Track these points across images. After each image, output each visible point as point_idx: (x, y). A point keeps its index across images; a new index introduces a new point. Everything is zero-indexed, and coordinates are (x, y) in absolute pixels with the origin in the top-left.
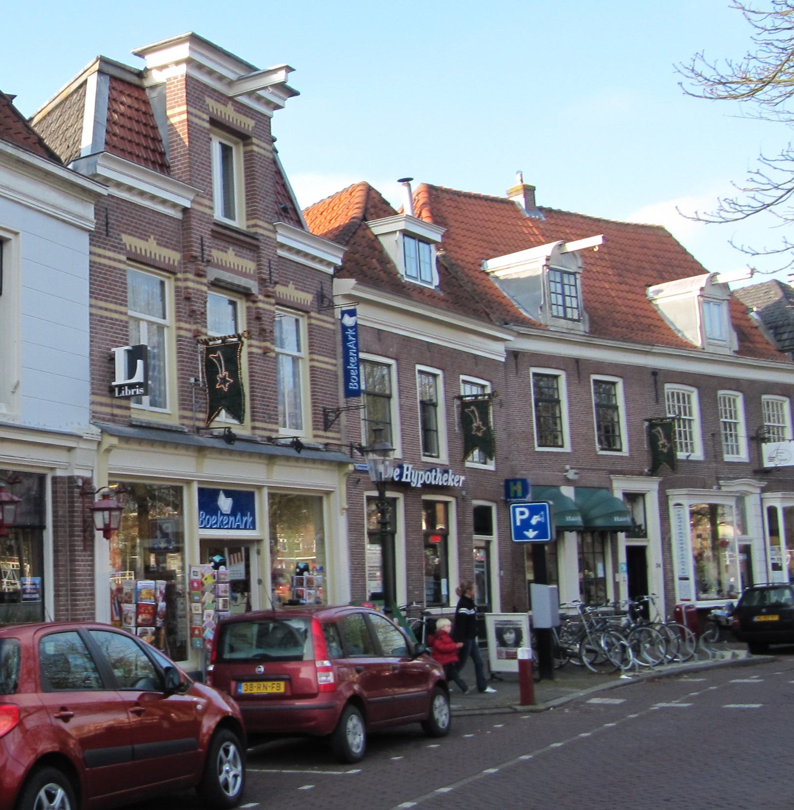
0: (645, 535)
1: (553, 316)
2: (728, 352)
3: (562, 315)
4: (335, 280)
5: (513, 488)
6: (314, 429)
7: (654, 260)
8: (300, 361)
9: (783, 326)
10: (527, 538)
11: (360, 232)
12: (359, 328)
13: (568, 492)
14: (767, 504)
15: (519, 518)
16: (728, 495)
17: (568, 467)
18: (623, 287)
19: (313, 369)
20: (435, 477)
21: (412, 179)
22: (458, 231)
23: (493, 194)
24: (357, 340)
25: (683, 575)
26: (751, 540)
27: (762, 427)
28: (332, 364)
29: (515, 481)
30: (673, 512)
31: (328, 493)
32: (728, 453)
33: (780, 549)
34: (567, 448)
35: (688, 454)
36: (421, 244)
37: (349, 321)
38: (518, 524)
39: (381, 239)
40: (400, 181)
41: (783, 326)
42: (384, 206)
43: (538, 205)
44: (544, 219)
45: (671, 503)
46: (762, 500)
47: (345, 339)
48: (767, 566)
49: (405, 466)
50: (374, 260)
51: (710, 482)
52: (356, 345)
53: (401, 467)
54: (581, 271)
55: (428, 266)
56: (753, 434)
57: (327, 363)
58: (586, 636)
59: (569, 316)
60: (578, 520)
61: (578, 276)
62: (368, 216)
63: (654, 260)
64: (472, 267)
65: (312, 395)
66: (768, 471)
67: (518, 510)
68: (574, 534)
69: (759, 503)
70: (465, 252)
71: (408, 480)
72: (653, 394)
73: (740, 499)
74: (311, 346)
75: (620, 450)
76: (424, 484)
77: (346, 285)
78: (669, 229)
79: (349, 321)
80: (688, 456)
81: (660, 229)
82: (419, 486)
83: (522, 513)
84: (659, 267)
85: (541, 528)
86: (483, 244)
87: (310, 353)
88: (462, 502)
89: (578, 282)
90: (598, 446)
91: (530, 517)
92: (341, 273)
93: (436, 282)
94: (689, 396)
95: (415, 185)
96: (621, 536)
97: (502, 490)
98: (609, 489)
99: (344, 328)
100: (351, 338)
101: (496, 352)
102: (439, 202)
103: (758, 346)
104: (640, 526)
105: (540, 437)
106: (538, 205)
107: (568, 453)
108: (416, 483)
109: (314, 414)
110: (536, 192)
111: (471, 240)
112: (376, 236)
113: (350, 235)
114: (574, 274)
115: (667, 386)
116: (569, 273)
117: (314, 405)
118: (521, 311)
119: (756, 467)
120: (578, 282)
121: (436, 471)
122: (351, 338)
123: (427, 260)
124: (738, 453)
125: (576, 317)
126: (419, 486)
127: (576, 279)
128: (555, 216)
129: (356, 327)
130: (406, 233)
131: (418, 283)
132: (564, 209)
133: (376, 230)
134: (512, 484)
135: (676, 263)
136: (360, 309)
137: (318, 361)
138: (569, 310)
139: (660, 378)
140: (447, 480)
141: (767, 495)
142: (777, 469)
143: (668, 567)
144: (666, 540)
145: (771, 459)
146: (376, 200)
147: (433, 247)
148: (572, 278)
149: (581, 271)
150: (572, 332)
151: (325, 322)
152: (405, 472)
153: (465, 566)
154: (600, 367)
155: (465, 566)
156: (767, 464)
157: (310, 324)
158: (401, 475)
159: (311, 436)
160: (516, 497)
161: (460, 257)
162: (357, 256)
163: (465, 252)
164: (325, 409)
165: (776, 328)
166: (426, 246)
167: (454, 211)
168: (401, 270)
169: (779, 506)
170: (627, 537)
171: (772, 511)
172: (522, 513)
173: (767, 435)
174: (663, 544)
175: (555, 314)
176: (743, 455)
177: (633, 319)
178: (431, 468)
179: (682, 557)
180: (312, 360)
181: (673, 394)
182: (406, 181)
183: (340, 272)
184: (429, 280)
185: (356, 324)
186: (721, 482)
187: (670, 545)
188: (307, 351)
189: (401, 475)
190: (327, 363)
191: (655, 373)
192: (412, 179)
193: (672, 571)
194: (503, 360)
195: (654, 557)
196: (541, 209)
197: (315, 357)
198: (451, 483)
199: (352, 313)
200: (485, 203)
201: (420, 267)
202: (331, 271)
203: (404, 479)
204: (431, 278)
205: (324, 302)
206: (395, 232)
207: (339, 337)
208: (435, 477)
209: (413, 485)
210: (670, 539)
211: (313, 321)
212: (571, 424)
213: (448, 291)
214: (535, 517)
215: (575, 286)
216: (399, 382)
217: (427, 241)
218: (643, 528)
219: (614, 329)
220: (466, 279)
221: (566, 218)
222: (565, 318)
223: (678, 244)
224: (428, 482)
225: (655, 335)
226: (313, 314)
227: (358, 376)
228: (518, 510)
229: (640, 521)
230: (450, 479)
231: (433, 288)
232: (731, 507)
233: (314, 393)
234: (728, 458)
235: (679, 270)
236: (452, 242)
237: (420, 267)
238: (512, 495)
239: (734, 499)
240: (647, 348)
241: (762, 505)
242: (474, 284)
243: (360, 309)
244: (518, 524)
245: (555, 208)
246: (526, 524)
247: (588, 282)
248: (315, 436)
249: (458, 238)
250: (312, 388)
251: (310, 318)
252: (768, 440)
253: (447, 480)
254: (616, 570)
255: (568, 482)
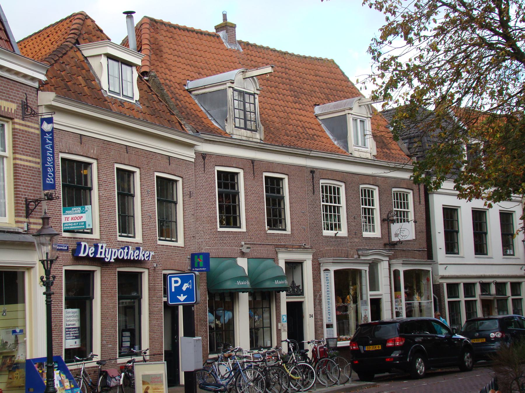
0: (302, 294)
1: (235, 127)
2: (369, 156)
3: (242, 126)
4: (39, 92)
5: (197, 260)
6: (16, 216)
7: (324, 85)
8: (5, 159)
9: (414, 137)
10: (180, 301)
11: (71, 53)
12: (55, 131)
13: (242, 262)
14: (393, 269)
15: (174, 285)
16: (364, 263)
17: (243, 243)
18: (297, 106)
19: (15, 166)
20: (128, 253)
21: (134, 12)
22: (171, 57)
23: (203, 29)
24: (53, 143)
25: (328, 323)
26: (381, 295)
27: (391, 212)
28: (32, 162)
29: (198, 255)
30: (323, 274)
31: (29, 269)
32: (366, 230)
33: (401, 301)
34: (244, 229)
35: (336, 232)
36: (123, 66)
37: (47, 127)
38: (173, 290)
39: (90, 60)
40: (125, 13)
41: (414, 137)
42: (99, 33)
43: (238, 38)
44: (241, 50)
45: (322, 269)
46: (390, 265)
47: (44, 142)
48: (392, 314)
49: (100, 245)
50: (80, 78)
51: (352, 253)
52: (52, 147)
53: (96, 246)
54: (258, 92)
55: (129, 84)
56: (385, 217)
57: (30, 161)
58: (240, 373)
59: (249, 127)
60: (247, 284)
61: (256, 96)
62: (81, 40)
63: (324, 85)
64: (178, 86)
65: (15, 188)
66: (394, 244)
67: (173, 279)
68: (247, 294)
69: (388, 267)
70: (174, 74)
71: (103, 256)
72: (311, 188)
73: (373, 266)
74: (14, 147)
75: (285, 230)
76: (117, 259)
77: (47, 98)
78: (337, 62)
79: (47, 127)
80: (336, 234)
81: (332, 61)
82: (112, 260)
83: (176, 282)
84: (326, 91)
85: (189, 293)
86: (188, 67)
87: (14, 153)
88: (153, 272)
89: (257, 101)
90: (267, 227)
91: (182, 285)
92: (45, 86)
93: (137, 97)
94: (338, 189)
95: (137, 19)
96: (283, 294)
97: (188, 262)
98: (275, 260)
99: (43, 132)
100: (48, 141)
101: (189, 155)
102: (152, 34)
103: (393, 151)
104: (299, 286)
105: (221, 222)
106: (238, 38)
107: (243, 232)
108: (109, 258)
109: (16, 203)
110: (237, 29)
111: (180, 65)
112: (86, 58)
113: (60, 55)
114: (254, 94)
115: (322, 181)
116: (250, 94)
117: (17, 196)
118: (213, 122)
119: (386, 241)
120: (257, 101)
121: (128, 249)
122: (48, 141)
123: (129, 79)
124: (374, 231)
125: (253, 128)
126: (112, 260)
127: (255, 98)
128: (251, 48)
129: (52, 132)
130: (110, 57)
131: (121, 97)
132: (258, 44)
133: (86, 53)
134: (196, 257)
135: (340, 88)
136: (57, 118)
137: (21, 159)
138: (248, 123)
139: (316, 175)
140: (139, 255)
141: (393, 261)
142: (400, 242)
143: (319, 317)
144: (318, 296)
145: (396, 235)
146: (91, 28)
147: (134, 69)
148: (252, 97)
149: (258, 92)
150: (251, 139)
151: (32, 128)
152: (100, 250)
153: (154, 322)
154: (270, 166)
155: (154, 322)
156: (394, 239)
157: (14, 129)
158: (96, 252)
159: (14, 222)
160: (199, 267)
161: (169, 78)
162: (63, 73)
163: (174, 74)
164: (26, 200)
165: (410, 138)
166: (129, 68)
167: (169, 40)
168: (105, 86)
169: (402, 269)
170: (287, 295)
171: (396, 273)
172: (176, 282)
173: (395, 218)
174: (315, 300)
175: (237, 125)
176: (377, 233)
177: (301, 130)
178: (125, 246)
179: (329, 309)
180: (15, 159)
181: (326, 187)
182: (129, 14)
183: (43, 86)
184: (131, 95)
185: (53, 128)
186: (360, 252)
187: (320, 300)
188: (11, 151)
189: (96, 252)
190: (30, 161)
191: (313, 171)
192: (134, 12)
193: (322, 320)
194: (193, 160)
195: (309, 309)
196: (240, 42)
197: (18, 156)
198: (141, 257)
199: (50, 121)
200: (196, 35)
201: (121, 83)
202: (36, 85)
203: (98, 256)
204: (133, 92)
205: (27, 110)
206: (100, 55)
207: (39, 142)
208: (128, 253)
209: (107, 260)
210: (320, 296)
211: (17, 126)
212: (246, 210)
213: (147, 104)
214: (185, 284)
215: (254, 104)
216: (99, 177)
217: (129, 64)
218: (301, 288)
219: (286, 137)
220: (170, 96)
221: (259, 50)
222: (245, 128)
223: (343, 74)
224: (121, 258)
225: (316, 143)
226: (16, 120)
227: (54, 172)
228: (173, 279)
229: (298, 283)
230: (141, 255)
231: (134, 102)
232: (366, 271)
233: (16, 187)
234: (366, 234)
235: (341, 94)
236: (164, 65)
237: (121, 83)
238: (196, 265)
239: (368, 265)
240: (307, 153)
241: (390, 269)
242: (177, 99)
243: (57, 118)
244: (173, 290)
245: (251, 42)
246: (179, 290)
247: (263, 100)
248: (17, 222)
249: (170, 62)
250: (15, 182)
251: (14, 123)
252: (393, 221)
253: (139, 255)
254: (278, 320)
255: (243, 255)
